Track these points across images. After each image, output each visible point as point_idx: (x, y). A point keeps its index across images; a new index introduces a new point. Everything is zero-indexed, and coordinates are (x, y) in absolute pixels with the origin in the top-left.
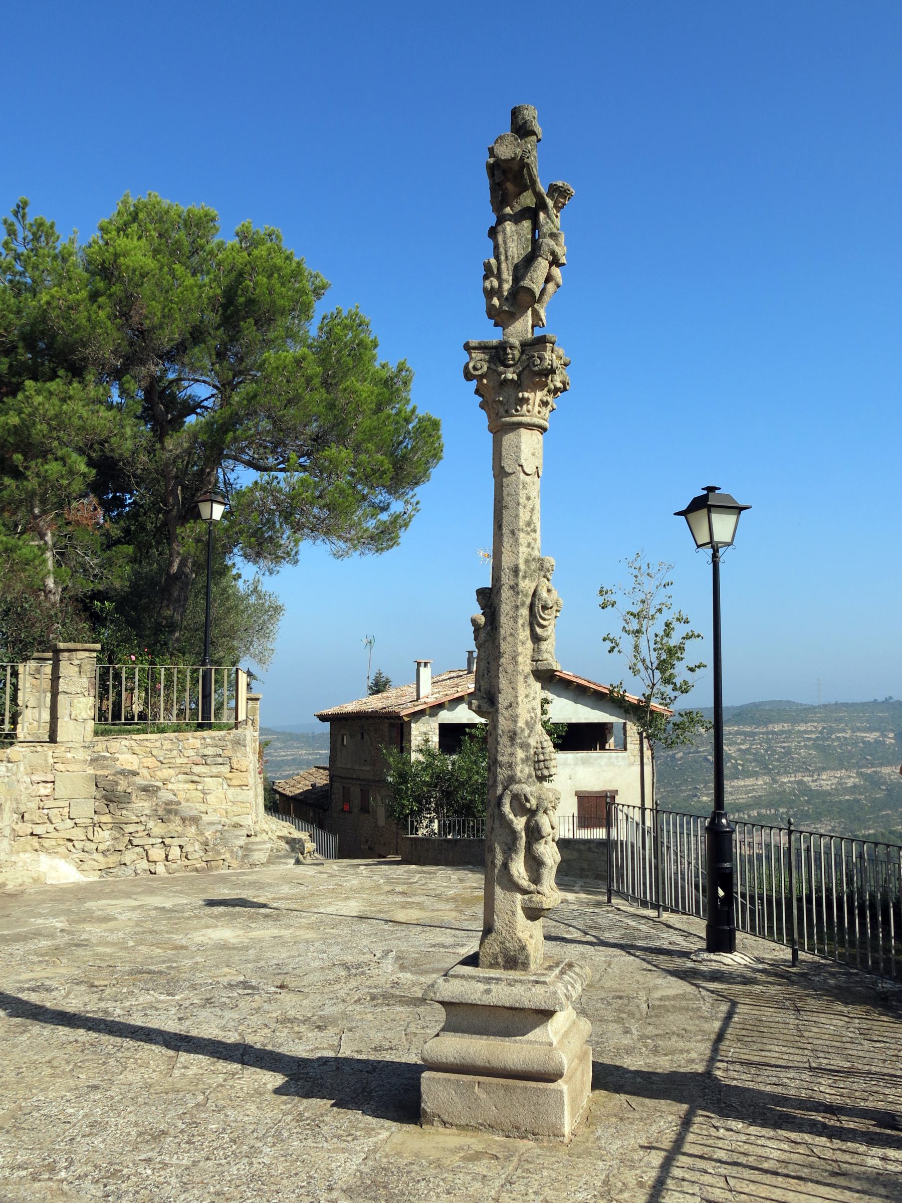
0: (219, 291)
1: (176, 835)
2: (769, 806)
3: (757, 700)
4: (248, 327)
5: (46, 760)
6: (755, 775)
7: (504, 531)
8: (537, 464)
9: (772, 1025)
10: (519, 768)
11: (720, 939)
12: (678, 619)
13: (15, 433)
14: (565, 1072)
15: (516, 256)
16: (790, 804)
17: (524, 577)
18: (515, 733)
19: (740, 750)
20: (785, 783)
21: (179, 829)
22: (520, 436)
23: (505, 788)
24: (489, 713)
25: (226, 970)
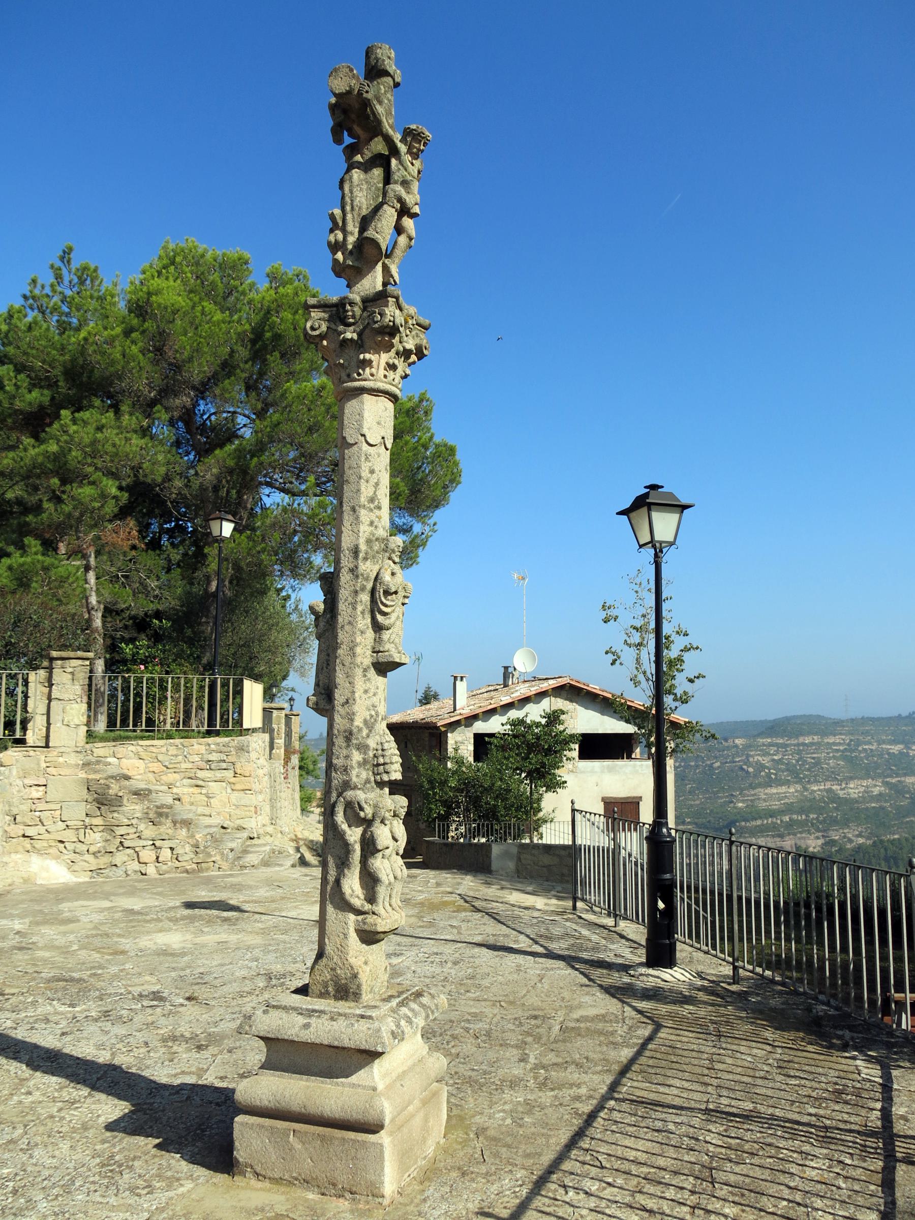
0: (247, 327)
1: (166, 837)
2: (801, 811)
3: (789, 714)
4: (274, 359)
5: (38, 764)
6: (787, 783)
7: (344, 508)
8: (382, 434)
9: (685, 1053)
10: (354, 773)
11: (661, 953)
12: (678, 633)
13: (54, 460)
14: (387, 1122)
15: (364, 206)
16: (820, 810)
17: (365, 559)
18: (351, 733)
19: (773, 760)
20: (815, 791)
21: (170, 831)
22: (363, 403)
23: (340, 795)
24: (327, 711)
25: (148, 978)
